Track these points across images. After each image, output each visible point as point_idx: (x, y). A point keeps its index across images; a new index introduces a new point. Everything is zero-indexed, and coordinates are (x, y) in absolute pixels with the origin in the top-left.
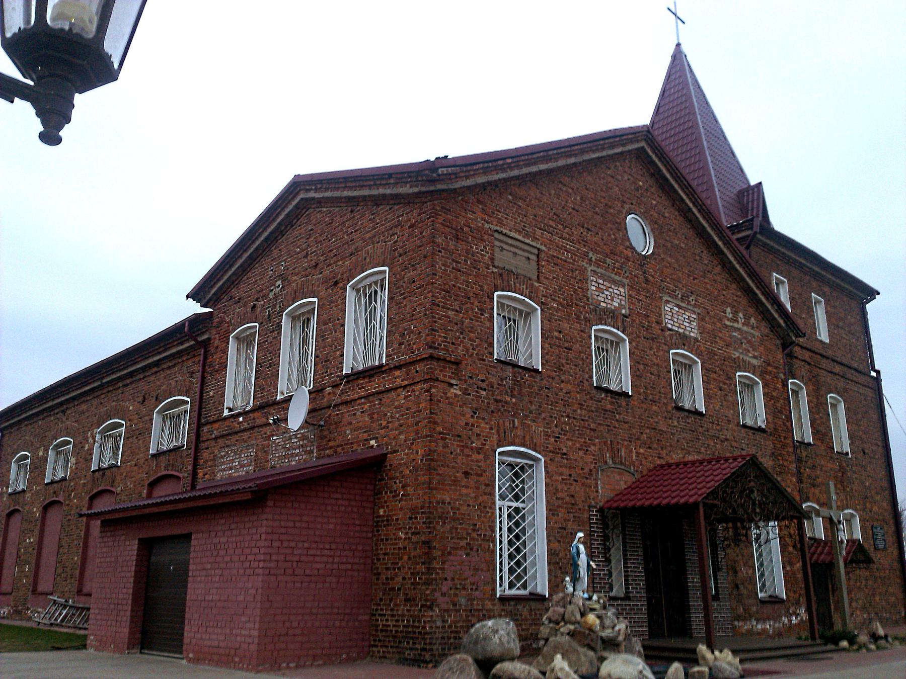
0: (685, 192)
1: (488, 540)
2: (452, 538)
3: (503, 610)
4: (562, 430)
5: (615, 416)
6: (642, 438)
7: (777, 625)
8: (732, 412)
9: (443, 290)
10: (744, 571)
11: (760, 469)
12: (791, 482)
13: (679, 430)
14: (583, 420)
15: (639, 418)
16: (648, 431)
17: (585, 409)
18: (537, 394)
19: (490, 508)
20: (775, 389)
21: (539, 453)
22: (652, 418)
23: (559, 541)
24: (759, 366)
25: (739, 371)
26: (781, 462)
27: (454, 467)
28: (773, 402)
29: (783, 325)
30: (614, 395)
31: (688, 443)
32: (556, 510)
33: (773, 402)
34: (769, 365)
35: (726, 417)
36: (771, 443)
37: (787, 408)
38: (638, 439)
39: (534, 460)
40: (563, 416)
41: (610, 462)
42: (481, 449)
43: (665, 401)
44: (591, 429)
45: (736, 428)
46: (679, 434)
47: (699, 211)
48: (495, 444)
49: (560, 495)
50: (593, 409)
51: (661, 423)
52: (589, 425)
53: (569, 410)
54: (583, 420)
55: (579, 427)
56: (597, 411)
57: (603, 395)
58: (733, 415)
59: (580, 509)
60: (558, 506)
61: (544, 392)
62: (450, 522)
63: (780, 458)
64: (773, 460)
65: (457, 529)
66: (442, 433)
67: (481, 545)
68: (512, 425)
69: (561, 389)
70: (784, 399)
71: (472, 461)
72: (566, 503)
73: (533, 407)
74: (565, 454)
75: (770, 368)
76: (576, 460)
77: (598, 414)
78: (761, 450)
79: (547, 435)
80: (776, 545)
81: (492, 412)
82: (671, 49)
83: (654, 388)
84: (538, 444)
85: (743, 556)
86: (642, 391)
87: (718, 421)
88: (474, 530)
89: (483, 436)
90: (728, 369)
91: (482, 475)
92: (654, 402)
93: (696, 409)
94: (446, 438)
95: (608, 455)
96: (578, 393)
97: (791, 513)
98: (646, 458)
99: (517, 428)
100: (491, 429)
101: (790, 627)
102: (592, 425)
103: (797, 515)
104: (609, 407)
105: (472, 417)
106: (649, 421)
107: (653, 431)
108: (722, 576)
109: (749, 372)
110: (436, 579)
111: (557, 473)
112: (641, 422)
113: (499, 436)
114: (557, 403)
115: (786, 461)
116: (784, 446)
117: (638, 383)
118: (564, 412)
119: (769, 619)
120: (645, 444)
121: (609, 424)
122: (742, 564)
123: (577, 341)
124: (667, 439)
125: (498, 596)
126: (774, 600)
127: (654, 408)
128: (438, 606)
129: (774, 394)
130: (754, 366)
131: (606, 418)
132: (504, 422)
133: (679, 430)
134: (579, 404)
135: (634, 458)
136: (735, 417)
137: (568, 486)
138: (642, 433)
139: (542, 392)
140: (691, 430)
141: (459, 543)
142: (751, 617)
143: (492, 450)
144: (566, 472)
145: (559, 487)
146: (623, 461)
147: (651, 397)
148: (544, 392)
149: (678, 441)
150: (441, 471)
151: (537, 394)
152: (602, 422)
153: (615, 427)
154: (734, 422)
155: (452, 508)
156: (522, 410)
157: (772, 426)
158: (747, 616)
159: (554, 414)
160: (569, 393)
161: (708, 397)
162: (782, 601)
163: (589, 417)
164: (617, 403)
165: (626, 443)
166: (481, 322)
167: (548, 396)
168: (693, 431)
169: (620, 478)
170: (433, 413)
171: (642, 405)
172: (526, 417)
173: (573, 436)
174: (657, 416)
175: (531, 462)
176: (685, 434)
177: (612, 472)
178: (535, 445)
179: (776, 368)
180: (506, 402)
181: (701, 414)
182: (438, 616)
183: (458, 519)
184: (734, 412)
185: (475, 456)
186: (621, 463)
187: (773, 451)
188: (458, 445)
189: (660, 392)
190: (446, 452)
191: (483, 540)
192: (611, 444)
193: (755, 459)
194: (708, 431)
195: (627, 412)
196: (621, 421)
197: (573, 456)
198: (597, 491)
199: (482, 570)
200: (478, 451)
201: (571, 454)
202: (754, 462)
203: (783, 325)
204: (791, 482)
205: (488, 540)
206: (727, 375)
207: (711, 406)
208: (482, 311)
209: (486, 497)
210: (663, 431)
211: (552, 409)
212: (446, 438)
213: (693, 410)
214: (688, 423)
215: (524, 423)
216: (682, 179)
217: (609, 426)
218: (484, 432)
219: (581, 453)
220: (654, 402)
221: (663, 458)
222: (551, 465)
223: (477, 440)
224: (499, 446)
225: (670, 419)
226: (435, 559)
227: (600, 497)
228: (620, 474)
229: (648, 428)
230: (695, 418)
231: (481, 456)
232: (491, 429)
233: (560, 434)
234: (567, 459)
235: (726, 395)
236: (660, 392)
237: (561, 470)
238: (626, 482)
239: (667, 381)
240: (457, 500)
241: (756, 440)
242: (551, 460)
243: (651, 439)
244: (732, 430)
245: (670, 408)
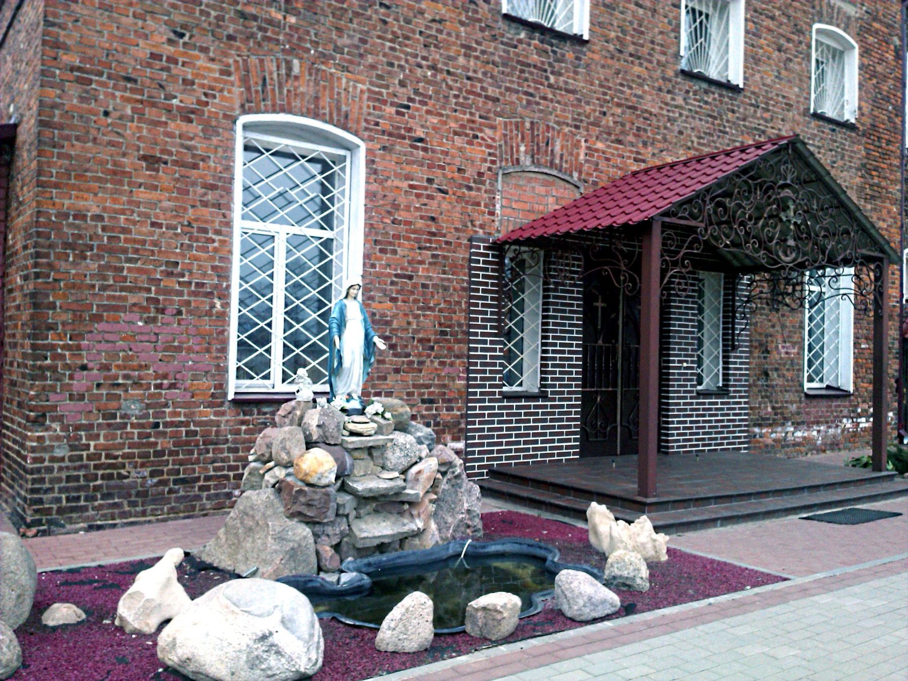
1: (209, 295)
2: (104, 288)
3: (243, 423)
4: (416, 92)
5: (547, 78)
6: (603, 123)
7: (831, 431)
8: (797, 90)
10: (781, 351)
11: (808, 165)
12: (889, 212)
13: (685, 113)
14: (469, 78)
15: (601, 86)
16: (619, 111)
17: (477, 58)
18: (357, 14)
19: (218, 232)
20: (882, 60)
21: (356, 134)
22: (630, 88)
23: (394, 300)
24: (857, 19)
25: (820, 22)
26: (876, 180)
27: (111, 144)
28: (874, 81)
30: (547, 38)
31: (700, 138)
32: (390, 243)
33: (874, 81)
34: (875, 19)
35: (784, 97)
36: (862, 147)
37: (899, 94)
38: (596, 124)
39: (348, 149)
40: (420, 66)
41: (526, 161)
42: (193, 112)
43: (663, 59)
44: (487, 97)
45: (800, 119)
46: (686, 122)
48: (237, 105)
49: (401, 216)
50: (497, 59)
51: (649, 98)
52: (482, 88)
53: (438, 57)
54: (469, 78)
55: (460, 90)
56: (505, 65)
57: (522, 35)
58: (798, 96)
59: (447, 243)
60: (397, 237)
61: (376, 12)
62: (100, 257)
63: (874, 173)
64: (862, 177)
66: (79, 69)
67: (188, 303)
68: (283, 71)
69: (422, 12)
70: (896, 79)
71: (171, 135)
72: (415, 232)
73: (346, 41)
74: (421, 140)
75: (877, 25)
76: (446, 153)
77: (507, 70)
78: (842, 159)
79: (378, 100)
80: (846, 311)
81: (230, 38)
83: (642, 33)
84: (354, 115)
85: (783, 326)
86: (613, 34)
87: (767, 104)
88: (170, 274)
89: (203, 86)
90: (799, 15)
91: (195, 166)
92: (639, 58)
93: (729, 81)
94: (90, 82)
95: (522, 148)
96: (462, 23)
97: (865, 252)
98: (608, 159)
99: (296, 78)
100: (226, 72)
101: (855, 434)
102: (490, 89)
103: (876, 254)
104: (535, 58)
105: (170, 42)
106: (622, 92)
107: (628, 111)
108: (740, 362)
109: (838, 26)
110: (53, 369)
111: (397, 175)
112: (605, 94)
113: (248, 89)
114: (407, 38)
115: (885, 178)
116: (885, 155)
117: (605, 19)
118: (424, 58)
119: (818, 423)
120: (609, 134)
121: (531, 91)
122: (780, 341)
124: (658, 128)
125: (231, 396)
126: (835, 394)
127: (637, 69)
128: (60, 419)
129: (879, 68)
130: (849, 18)
131: (526, 80)
132: (262, 61)
133: (685, 113)
134: (463, 46)
135: (582, 157)
136: (802, 100)
137: (425, 201)
138: (604, 114)
139: (369, 12)
140: (710, 116)
141: (125, 299)
142: (786, 419)
143: (226, 116)
144: (421, 174)
145: (402, 200)
146: (557, 161)
147: (631, 49)
148: (376, 12)
149: (681, 133)
150: (75, 149)
151: (357, 14)
152: (515, 86)
153: (545, 98)
154: (798, 108)
155: (104, 229)
156: (316, 44)
157: (868, 121)
158: (780, 418)
159: (399, 59)
160: (440, 22)
161: (752, 59)
162: (846, 395)
163: (485, 74)
164: (554, 52)
165: (567, 129)
167: (385, 22)
168: (715, 118)
169: (547, 191)
170: (53, 24)
171: (610, 61)
172: (325, 58)
173: (444, 108)
174: (641, 85)
175: (342, 152)
176: (697, 121)
177: (530, 180)
178: (346, 117)
179: (888, 26)
180: (271, 22)
181: (735, 89)
182: (58, 438)
183: (125, 251)
184: (802, 90)
185: (176, 126)
186: (552, 165)
187: (865, 161)
189: (652, 42)
190: (91, 112)
191: (195, 294)
192: (532, 129)
193: (799, 145)
194: (744, 120)
195: (576, 73)
196: (560, 89)
197: (441, 144)
198: (492, 213)
199: (190, 350)
200: (187, 115)
201: (435, 141)
202: (795, 150)
204: (889, 212)
205: (209, 295)
206: (796, 25)
207: (757, 77)
209: (206, 212)
210: (651, 114)
211: (392, 49)
212: (90, 82)
213: (724, 81)
214: (706, 103)
215: (318, 70)
217: (531, 95)
218: (204, 77)
219: (459, 141)
220: (639, 58)
221: (644, 161)
222: (383, 158)
223: (184, 91)
224: (245, 111)
225: (669, 92)
226: (52, 327)
227: (497, 224)
228: (546, 184)
229: (619, 105)
230: (720, 95)
231: (195, 128)
232: (226, 72)
233: (410, 99)
234: (425, 150)
235: (791, 60)
236: (652, 42)
237: (408, 169)
238: (558, 199)
239: (670, 23)
240: (123, 212)
241: (835, 141)
242: (384, 148)
243: (623, 125)
244: (794, 120)
245: (670, 73)
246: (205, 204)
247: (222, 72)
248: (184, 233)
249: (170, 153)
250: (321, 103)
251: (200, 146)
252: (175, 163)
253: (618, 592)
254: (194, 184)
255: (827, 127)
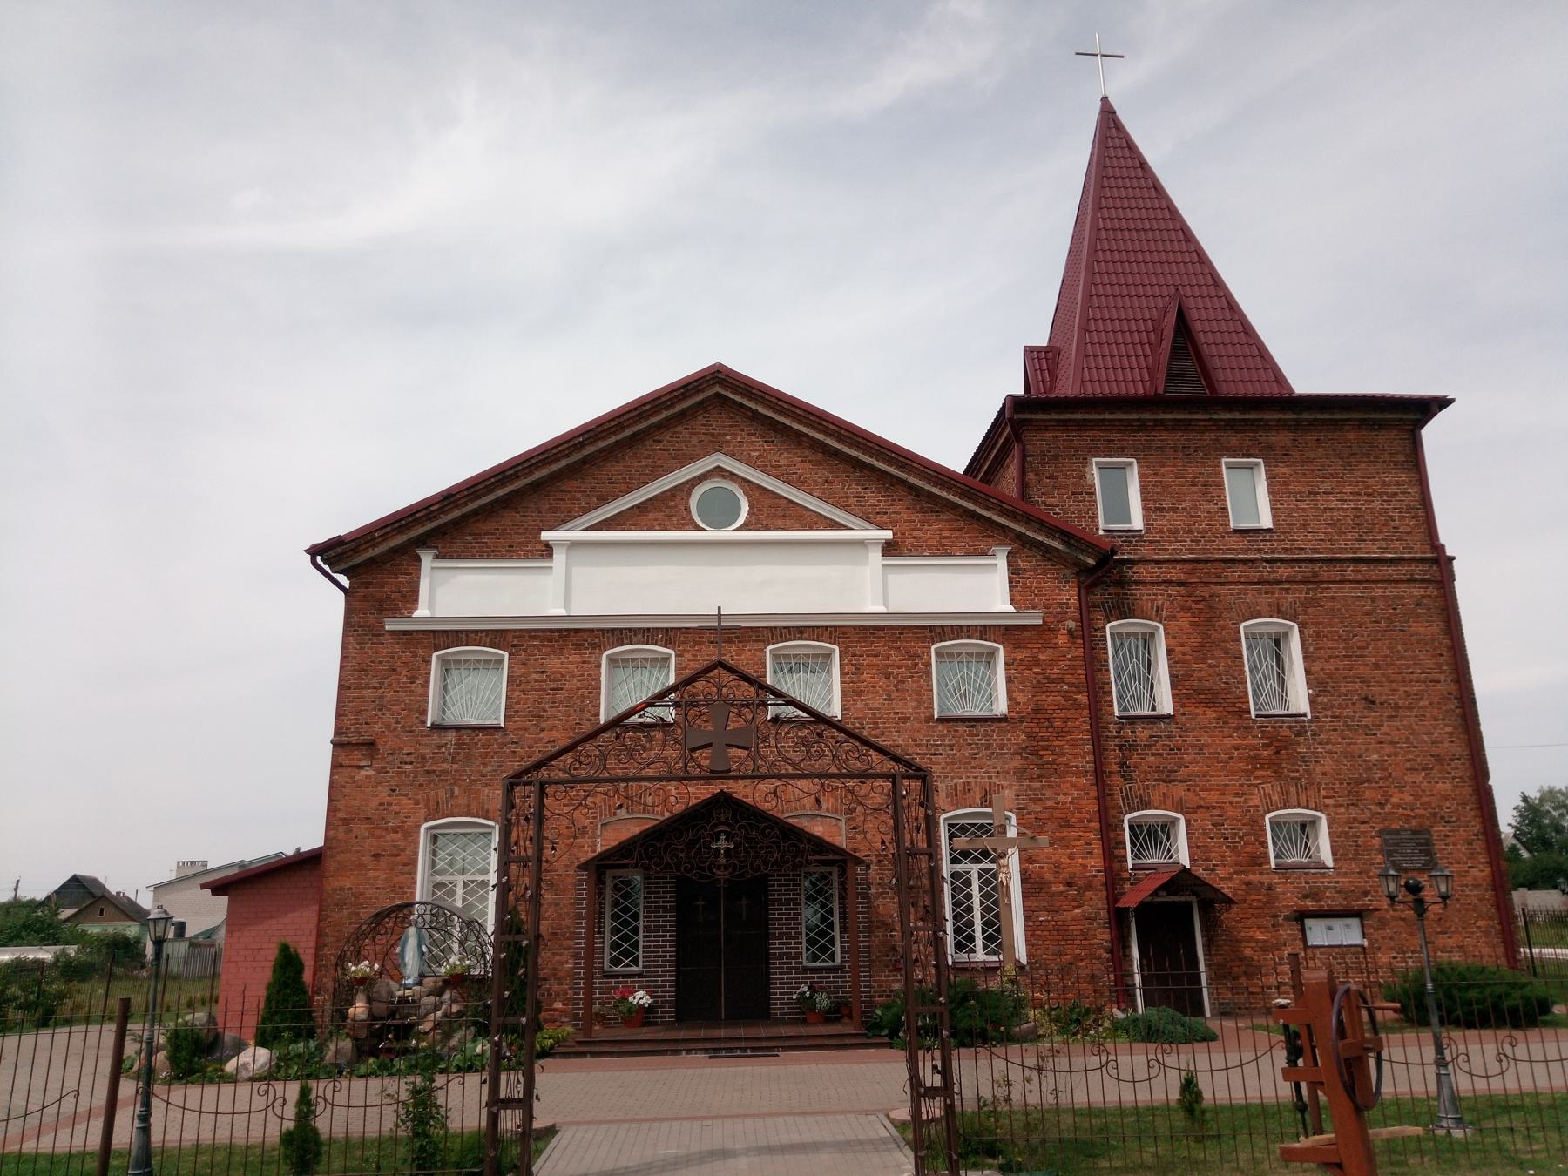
0: (805, 425)
9: (356, 671)
27: (358, 852)
29: (1060, 547)
42: (398, 827)
47: (839, 440)
65: (358, 913)
68: (449, 795)
81: (421, 785)
82: (1096, 108)
91: (398, 855)
100: (418, 804)
105: (389, 795)
110: (326, 966)
113: (429, 809)
123: (574, 676)
148: (509, 748)
166: (412, 691)
188: (367, 829)
203: (1060, 547)
208: (413, 679)
209: (402, 878)
216: (792, 409)
231: (399, 835)
246: (403, 874)
247: (415, 804)
248: (392, 891)
249: (385, 850)
250: (472, 807)
251: (402, 844)
252: (388, 855)
253: (540, 1130)
254: (397, 865)
255: (962, 728)
